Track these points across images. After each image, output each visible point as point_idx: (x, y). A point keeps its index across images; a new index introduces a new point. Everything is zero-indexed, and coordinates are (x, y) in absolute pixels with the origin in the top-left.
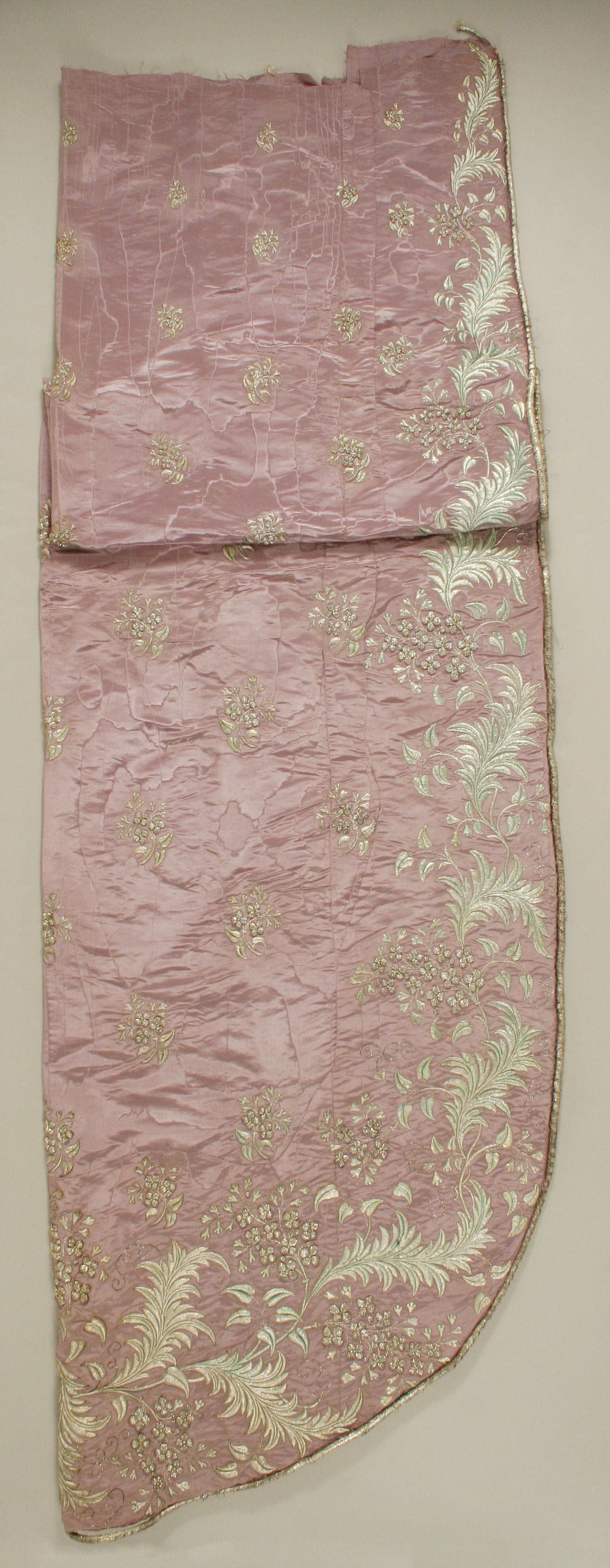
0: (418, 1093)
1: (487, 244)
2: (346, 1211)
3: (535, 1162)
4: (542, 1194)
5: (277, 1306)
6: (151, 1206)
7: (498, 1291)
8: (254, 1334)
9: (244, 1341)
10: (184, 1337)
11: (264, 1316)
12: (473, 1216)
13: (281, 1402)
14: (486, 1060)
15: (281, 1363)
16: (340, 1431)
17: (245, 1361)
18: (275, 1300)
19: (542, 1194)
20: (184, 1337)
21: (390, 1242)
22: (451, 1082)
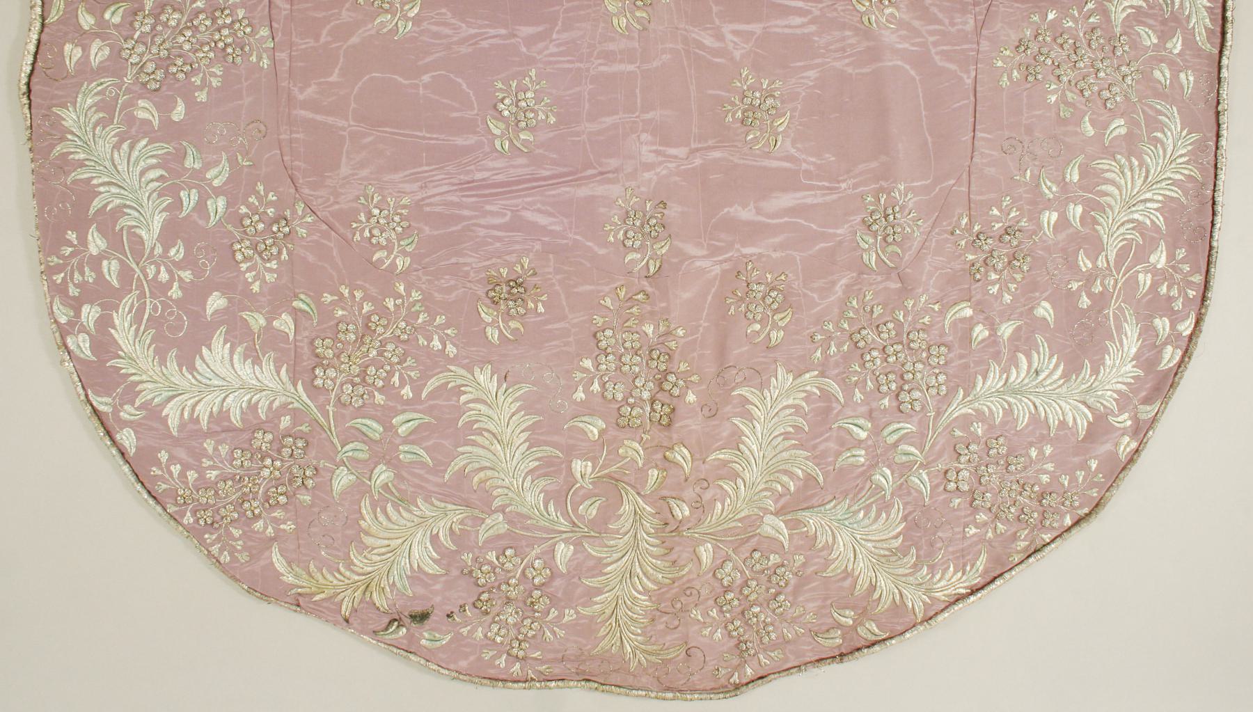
0: (1066, 194)
1: (1162, 128)
2: (980, 332)
3: (1190, 284)
4: (1198, 322)
5: (896, 445)
6: (755, 321)
7: (1142, 430)
8: (870, 477)
9: (851, 485)
10: (153, 174)
11: (880, 454)
12: (1121, 344)
13: (894, 558)
14: (1140, 166)
15: (897, 512)
16: (963, 591)
17: (856, 507)
18: (895, 437)
19: (1198, 322)
20: (153, 174)
21: (1028, 372)
22: (1104, 187)
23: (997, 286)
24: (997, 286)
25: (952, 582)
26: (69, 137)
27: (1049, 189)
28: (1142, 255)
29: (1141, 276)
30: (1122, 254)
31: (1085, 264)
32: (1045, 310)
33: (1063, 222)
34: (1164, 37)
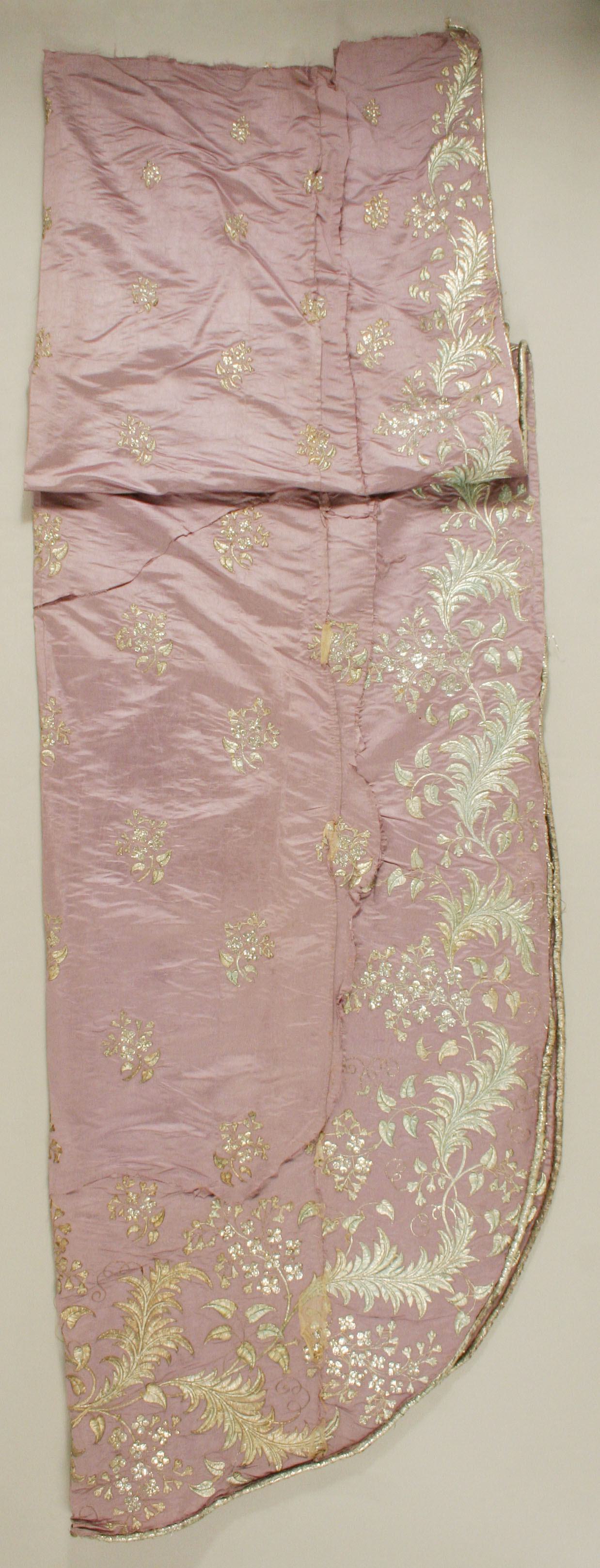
23: (394, 1015)
24: (394, 1015)
25: (298, 1442)
26: (438, 363)
27: (386, 1103)
28: (474, 1156)
29: (472, 1177)
30: (454, 1163)
31: (420, 1168)
32: (385, 1209)
33: (399, 1133)
34: (492, 964)
